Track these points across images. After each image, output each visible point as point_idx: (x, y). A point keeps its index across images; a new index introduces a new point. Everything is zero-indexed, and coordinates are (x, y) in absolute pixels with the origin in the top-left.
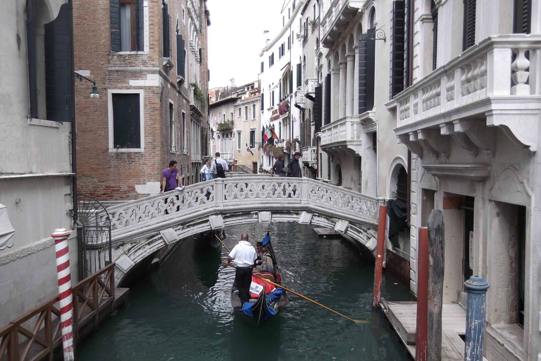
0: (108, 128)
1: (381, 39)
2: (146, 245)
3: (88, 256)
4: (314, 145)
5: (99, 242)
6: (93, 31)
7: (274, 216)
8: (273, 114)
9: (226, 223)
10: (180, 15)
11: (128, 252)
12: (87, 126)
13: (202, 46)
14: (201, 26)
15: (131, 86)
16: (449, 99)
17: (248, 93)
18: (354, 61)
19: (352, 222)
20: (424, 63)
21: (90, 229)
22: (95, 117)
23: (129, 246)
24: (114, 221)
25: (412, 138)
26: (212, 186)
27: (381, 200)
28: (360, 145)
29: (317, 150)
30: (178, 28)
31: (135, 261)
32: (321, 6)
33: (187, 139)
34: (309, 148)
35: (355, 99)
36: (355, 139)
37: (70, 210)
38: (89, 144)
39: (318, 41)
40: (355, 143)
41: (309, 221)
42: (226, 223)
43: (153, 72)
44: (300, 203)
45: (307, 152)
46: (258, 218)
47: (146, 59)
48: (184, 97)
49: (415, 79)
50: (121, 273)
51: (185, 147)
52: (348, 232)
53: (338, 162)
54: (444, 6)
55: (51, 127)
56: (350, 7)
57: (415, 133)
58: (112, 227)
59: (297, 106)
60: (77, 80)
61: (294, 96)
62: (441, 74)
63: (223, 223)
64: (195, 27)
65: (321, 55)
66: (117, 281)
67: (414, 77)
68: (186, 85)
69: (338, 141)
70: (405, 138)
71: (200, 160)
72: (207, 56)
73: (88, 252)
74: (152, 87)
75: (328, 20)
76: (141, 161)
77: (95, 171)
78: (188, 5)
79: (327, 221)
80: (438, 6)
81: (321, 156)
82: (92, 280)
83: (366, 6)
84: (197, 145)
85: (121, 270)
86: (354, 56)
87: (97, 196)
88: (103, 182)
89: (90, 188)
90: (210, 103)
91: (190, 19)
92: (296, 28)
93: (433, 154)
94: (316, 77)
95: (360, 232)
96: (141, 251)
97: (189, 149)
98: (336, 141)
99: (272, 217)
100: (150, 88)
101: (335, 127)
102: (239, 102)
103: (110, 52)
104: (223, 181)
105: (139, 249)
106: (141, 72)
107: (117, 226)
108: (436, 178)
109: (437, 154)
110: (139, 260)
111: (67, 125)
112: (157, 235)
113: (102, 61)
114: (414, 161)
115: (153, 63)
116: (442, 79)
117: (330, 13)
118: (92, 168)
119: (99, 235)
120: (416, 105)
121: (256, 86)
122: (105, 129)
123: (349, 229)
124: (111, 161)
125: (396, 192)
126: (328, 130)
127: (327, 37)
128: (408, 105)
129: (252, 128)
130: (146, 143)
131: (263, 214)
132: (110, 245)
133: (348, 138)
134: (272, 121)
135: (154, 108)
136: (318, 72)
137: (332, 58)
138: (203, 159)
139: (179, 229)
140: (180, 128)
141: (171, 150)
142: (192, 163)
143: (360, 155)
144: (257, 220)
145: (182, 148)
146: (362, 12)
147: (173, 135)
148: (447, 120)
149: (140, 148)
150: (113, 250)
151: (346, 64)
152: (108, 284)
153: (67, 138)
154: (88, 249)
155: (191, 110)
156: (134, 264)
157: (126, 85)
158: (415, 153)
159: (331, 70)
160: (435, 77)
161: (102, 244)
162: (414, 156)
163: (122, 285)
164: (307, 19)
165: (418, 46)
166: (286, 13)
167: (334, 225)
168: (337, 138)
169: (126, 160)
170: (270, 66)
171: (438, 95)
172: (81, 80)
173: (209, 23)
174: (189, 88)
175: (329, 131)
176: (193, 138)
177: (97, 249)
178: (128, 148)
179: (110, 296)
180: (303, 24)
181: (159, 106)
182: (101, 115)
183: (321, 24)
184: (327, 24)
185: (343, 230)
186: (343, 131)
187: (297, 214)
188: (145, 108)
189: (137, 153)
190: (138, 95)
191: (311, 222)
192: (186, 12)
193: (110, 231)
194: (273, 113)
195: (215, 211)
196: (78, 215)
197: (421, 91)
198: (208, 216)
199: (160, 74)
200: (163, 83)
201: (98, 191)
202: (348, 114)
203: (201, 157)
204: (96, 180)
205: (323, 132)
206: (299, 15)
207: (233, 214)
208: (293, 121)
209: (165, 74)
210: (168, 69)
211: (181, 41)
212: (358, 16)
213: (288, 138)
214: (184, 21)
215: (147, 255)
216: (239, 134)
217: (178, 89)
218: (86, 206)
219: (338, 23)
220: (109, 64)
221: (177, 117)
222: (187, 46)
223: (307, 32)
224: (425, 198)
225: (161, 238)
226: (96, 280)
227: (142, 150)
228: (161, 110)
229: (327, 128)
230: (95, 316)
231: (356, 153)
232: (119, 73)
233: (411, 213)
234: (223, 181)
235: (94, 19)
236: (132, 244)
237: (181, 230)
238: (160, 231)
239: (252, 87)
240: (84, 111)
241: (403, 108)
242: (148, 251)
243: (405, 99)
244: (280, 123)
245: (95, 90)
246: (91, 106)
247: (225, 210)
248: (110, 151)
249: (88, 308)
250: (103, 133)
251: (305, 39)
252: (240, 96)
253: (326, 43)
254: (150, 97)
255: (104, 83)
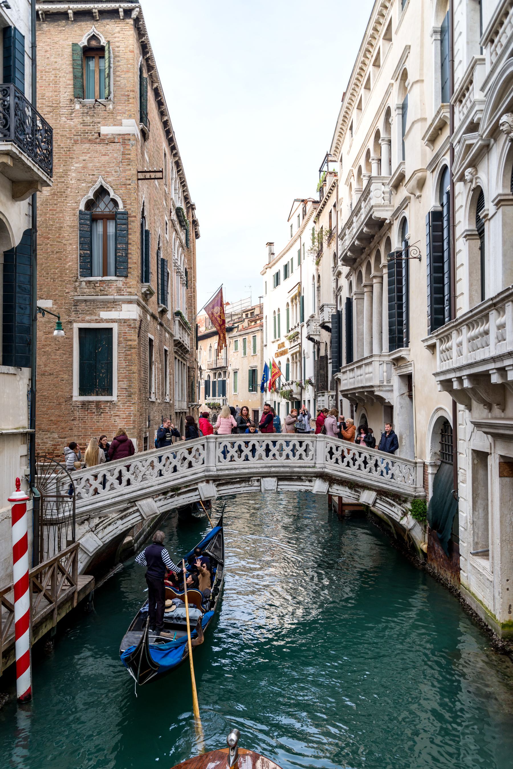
0: (72, 370)
1: (415, 258)
2: (118, 519)
3: (45, 533)
4: (332, 389)
5: (61, 515)
6: (57, 252)
7: (280, 483)
8: (279, 348)
9: (221, 492)
10: (162, 230)
11: (96, 529)
12: (47, 369)
13: (189, 265)
14: (187, 240)
15: (102, 319)
16: (500, 338)
17: (246, 320)
18: (382, 283)
19: (382, 493)
20: (470, 290)
21: (49, 499)
22: (58, 357)
23: (96, 521)
24: (79, 489)
25: (456, 386)
26: (220, 461)
27: (420, 463)
28: (392, 391)
29: (337, 395)
30: (161, 245)
31: (103, 540)
32: (339, 213)
33: (170, 383)
34: (326, 394)
35: (383, 331)
36: (385, 383)
37: (26, 475)
38: (49, 390)
39: (335, 255)
40: (384, 389)
41: (325, 491)
42: (221, 492)
43: (130, 302)
44: (314, 467)
45: (323, 398)
46: (260, 486)
47: (121, 286)
48: (166, 330)
49: (460, 308)
50: (85, 555)
51: (168, 393)
52: (377, 505)
53: (364, 412)
54: (492, 221)
55: (7, 374)
56: (375, 217)
57: (460, 379)
58: (76, 498)
59: (310, 338)
60: (39, 315)
61: (305, 325)
62: (490, 307)
63: (215, 492)
64: (181, 242)
65: (340, 274)
66: (80, 566)
67: (458, 307)
68: (169, 315)
69: (362, 385)
70: (447, 385)
71: (186, 408)
72: (195, 277)
73: (45, 528)
74: (129, 320)
75: (347, 232)
76: (112, 412)
77: (56, 424)
78: (172, 216)
79: (349, 491)
80: (484, 220)
81: (341, 403)
82: (50, 565)
83: (395, 215)
84: (182, 390)
85: (85, 552)
86: (382, 277)
87: (56, 456)
88: (65, 438)
89: (48, 445)
90: (199, 335)
91: (174, 233)
92: (307, 238)
93: (484, 405)
94: (333, 302)
95: (392, 505)
96: (110, 528)
97: (172, 395)
98: (360, 385)
99: (278, 485)
100: (125, 321)
101: (359, 367)
102: (235, 333)
103: (77, 278)
104: (216, 438)
105: (109, 525)
106: (114, 302)
107: (82, 495)
108: (489, 436)
109: (489, 407)
110: (108, 539)
111: (26, 371)
112: (132, 507)
113: (66, 288)
114: (461, 413)
115: (129, 290)
116: (490, 313)
117: (349, 224)
118: (51, 420)
119: (61, 507)
120: (460, 344)
121: (257, 312)
122: (69, 371)
123: (378, 501)
124: (75, 412)
125: (439, 453)
126: (350, 370)
127: (346, 253)
128: (450, 343)
129: (252, 365)
130: (120, 389)
131: (267, 481)
132: (74, 519)
133: (376, 382)
134: (278, 356)
135: (131, 345)
136: (337, 296)
137: (354, 279)
138: (189, 408)
139: (160, 500)
140: (162, 369)
141: (150, 398)
142: (176, 413)
143: (392, 404)
144: (259, 488)
145: (164, 394)
146: (390, 222)
147: (153, 379)
148: (499, 365)
149: (112, 395)
150: (77, 525)
151: (372, 286)
152: (69, 569)
153: (26, 386)
154: (46, 525)
155: (176, 345)
156: (102, 544)
157: (97, 317)
158: (461, 403)
159: (352, 294)
160: (481, 311)
161: (64, 519)
162: (460, 407)
163: (86, 572)
164: (322, 228)
165: (461, 268)
166: (294, 220)
167: (359, 496)
168: (361, 381)
169: (94, 410)
170: (275, 287)
171: (487, 333)
172: (43, 315)
173: (197, 236)
174: (173, 318)
175: (351, 373)
176: (177, 380)
177: (56, 524)
178: (97, 395)
179: (72, 585)
180: (316, 236)
181: (136, 343)
182: (65, 354)
183: (338, 237)
184: (347, 237)
185: (371, 502)
186: (369, 373)
187: (310, 481)
188: (118, 346)
189: (108, 402)
190: (111, 329)
191: (328, 491)
192: (170, 224)
193: (74, 502)
194: (279, 347)
195: (206, 476)
196: (36, 481)
197: (465, 326)
198: (197, 483)
199: (139, 304)
200: (142, 315)
201: (58, 450)
202: (376, 351)
203: (188, 405)
204: (56, 436)
205: (344, 373)
206: (311, 224)
207: (228, 480)
208: (304, 358)
209: (144, 303)
210: (148, 296)
211: (163, 264)
212: (385, 227)
213: (299, 379)
214: (167, 236)
215: (119, 532)
216: (235, 373)
217: (159, 320)
218: (44, 469)
219: (361, 237)
220: (76, 291)
221: (158, 355)
222: (171, 267)
223: (322, 245)
224: (476, 462)
225: (138, 510)
226: (56, 565)
227: (114, 398)
228: (139, 348)
229: (348, 368)
230: (54, 610)
231: (387, 401)
232: (88, 304)
233: (459, 481)
234: (216, 438)
235: (59, 237)
236: (100, 518)
237: (162, 501)
238: (136, 503)
239: (252, 313)
240: (43, 350)
241: (443, 347)
242: (120, 527)
243: (447, 336)
244: (288, 360)
245: (59, 327)
246: (52, 344)
247: (218, 476)
248: (74, 399)
249: (46, 602)
250: (66, 377)
251: (319, 254)
252: (236, 325)
253: (346, 260)
254: (126, 333)
255: (69, 316)
